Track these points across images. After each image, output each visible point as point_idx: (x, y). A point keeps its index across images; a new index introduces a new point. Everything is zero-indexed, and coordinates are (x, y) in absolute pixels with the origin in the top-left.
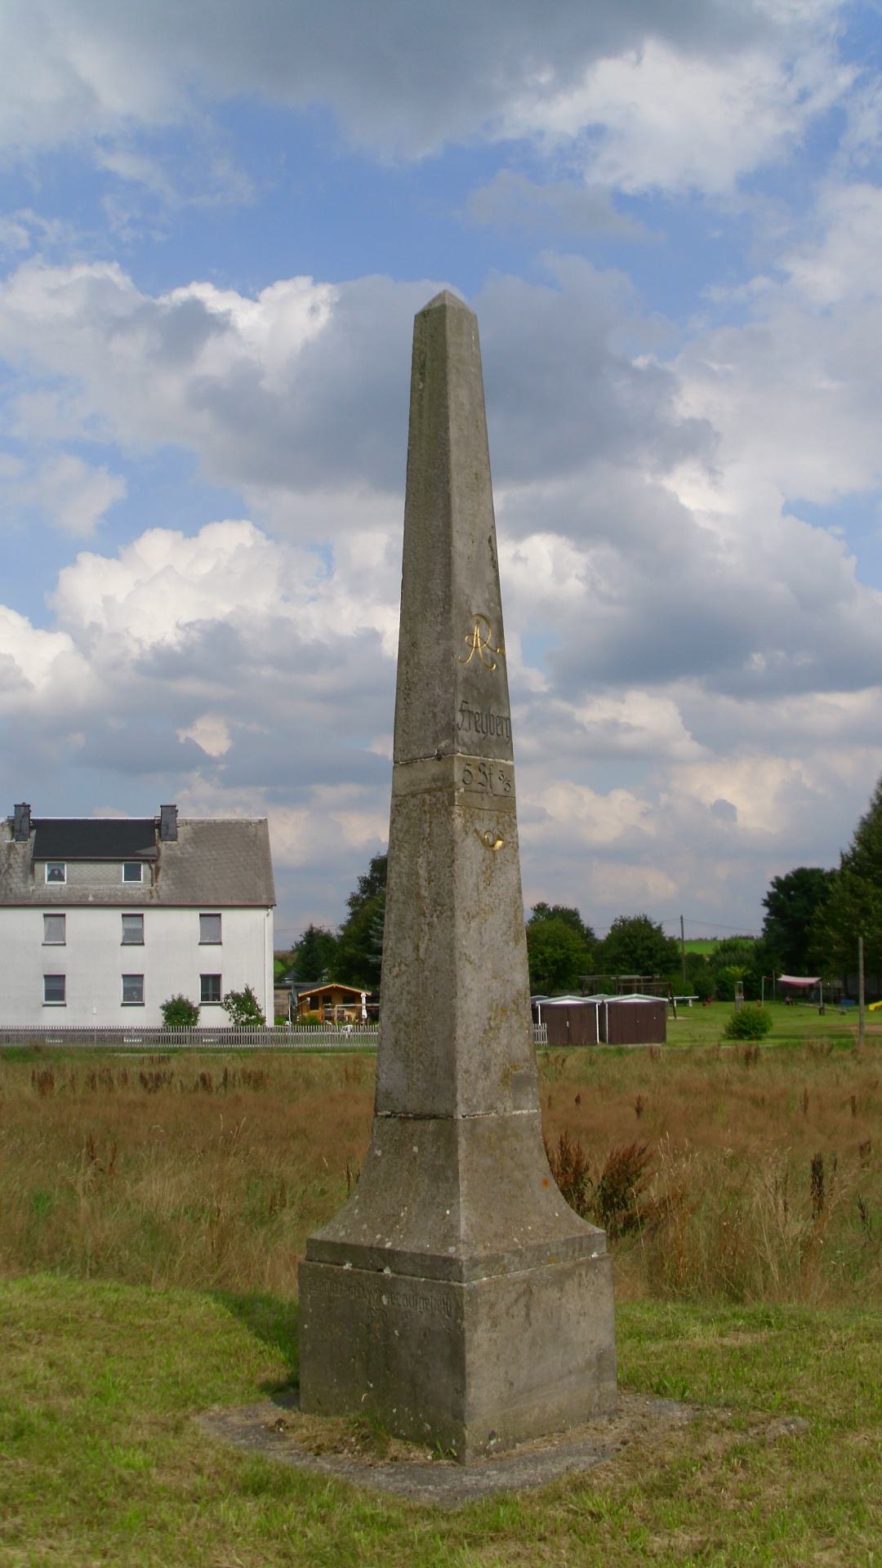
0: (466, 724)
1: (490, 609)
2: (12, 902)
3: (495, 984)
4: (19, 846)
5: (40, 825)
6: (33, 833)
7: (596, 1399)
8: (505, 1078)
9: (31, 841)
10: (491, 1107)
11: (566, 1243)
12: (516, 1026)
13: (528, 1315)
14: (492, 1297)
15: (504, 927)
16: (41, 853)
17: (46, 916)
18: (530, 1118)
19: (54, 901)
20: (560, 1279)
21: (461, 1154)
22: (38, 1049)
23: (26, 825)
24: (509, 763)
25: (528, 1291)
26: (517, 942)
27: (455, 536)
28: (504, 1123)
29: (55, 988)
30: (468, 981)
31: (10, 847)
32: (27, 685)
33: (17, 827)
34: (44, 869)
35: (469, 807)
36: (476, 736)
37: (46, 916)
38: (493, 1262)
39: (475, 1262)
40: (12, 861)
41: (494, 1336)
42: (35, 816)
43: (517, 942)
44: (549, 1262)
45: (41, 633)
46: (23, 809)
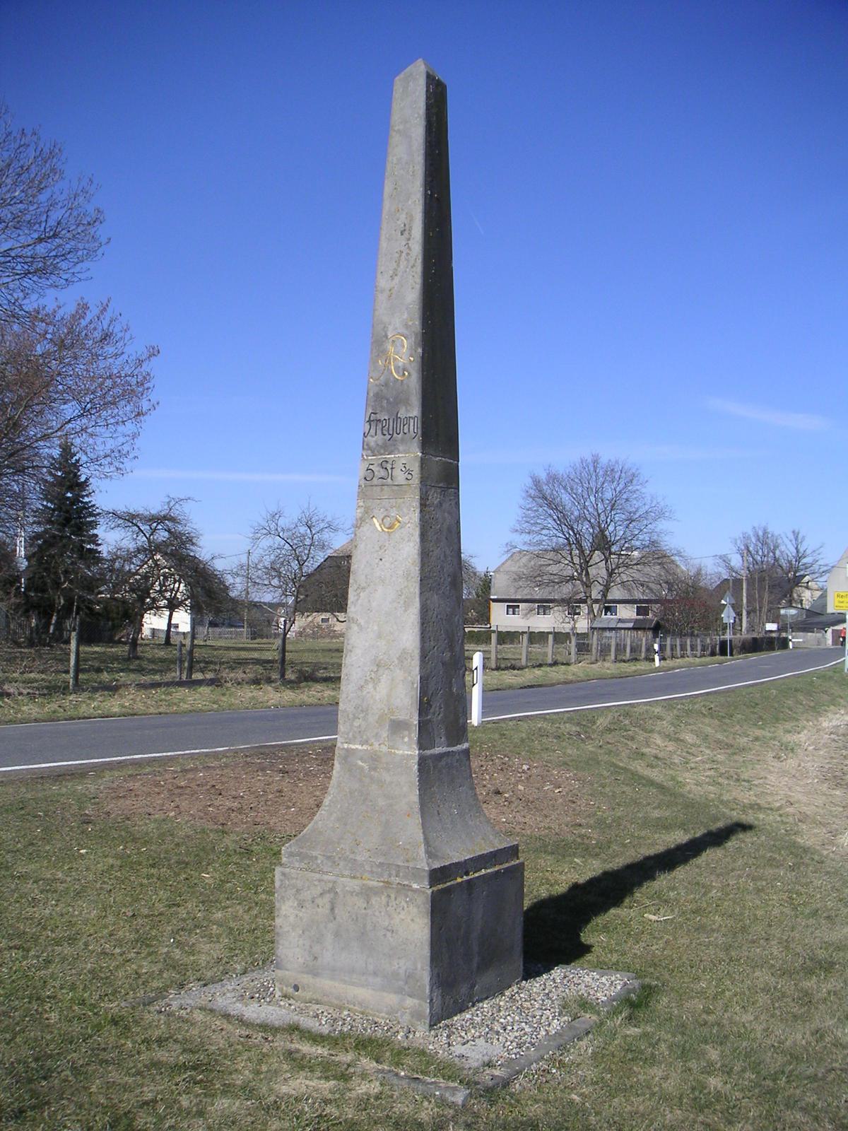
13: (332, 909)
41: (301, 914)
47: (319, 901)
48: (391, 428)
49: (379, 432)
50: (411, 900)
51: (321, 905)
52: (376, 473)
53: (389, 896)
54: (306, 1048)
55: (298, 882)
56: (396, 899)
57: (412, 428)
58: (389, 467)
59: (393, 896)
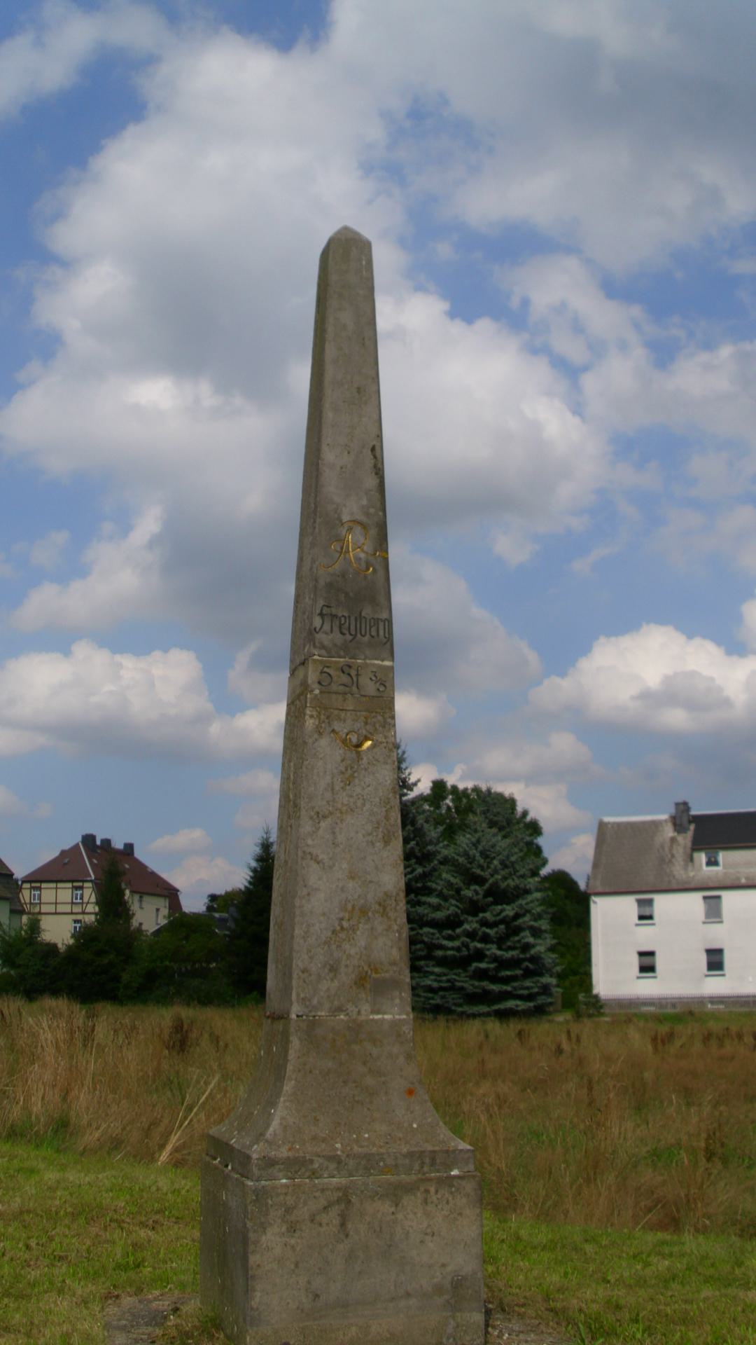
0: (327, 627)
1: (368, 515)
2: (675, 887)
3: (351, 884)
4: (680, 838)
5: (700, 820)
6: (692, 827)
7: (450, 1329)
8: (361, 981)
9: (690, 833)
10: (340, 1009)
11: (410, 1155)
12: (380, 928)
13: (343, 1225)
14: (290, 1200)
15: (369, 828)
16: (698, 844)
17: (705, 898)
18: (394, 1024)
19: (711, 885)
20: (396, 1193)
21: (292, 1055)
22: (691, 1013)
23: (685, 819)
24: (387, 663)
25: (344, 1198)
26: (387, 842)
27: (324, 448)
28: (356, 1029)
29: (715, 960)
30: (313, 880)
31: (673, 840)
32: (727, 703)
33: (678, 822)
34: (702, 857)
35: (326, 709)
36: (338, 638)
37: (705, 898)
38: (295, 1165)
39: (269, 1163)
40: (674, 852)
41: (293, 1241)
42: (694, 812)
43: (387, 842)
44: (382, 1173)
45: (735, 658)
46: (683, 807)
47: (324, 1218)
48: (353, 627)
49: (336, 629)
50: (458, 1190)
51: (324, 1221)
52: (335, 679)
53: (427, 1191)
54: (521, 1005)
55: (288, 1198)
56: (437, 1192)
57: (381, 632)
58: (353, 673)
59: (432, 1190)
